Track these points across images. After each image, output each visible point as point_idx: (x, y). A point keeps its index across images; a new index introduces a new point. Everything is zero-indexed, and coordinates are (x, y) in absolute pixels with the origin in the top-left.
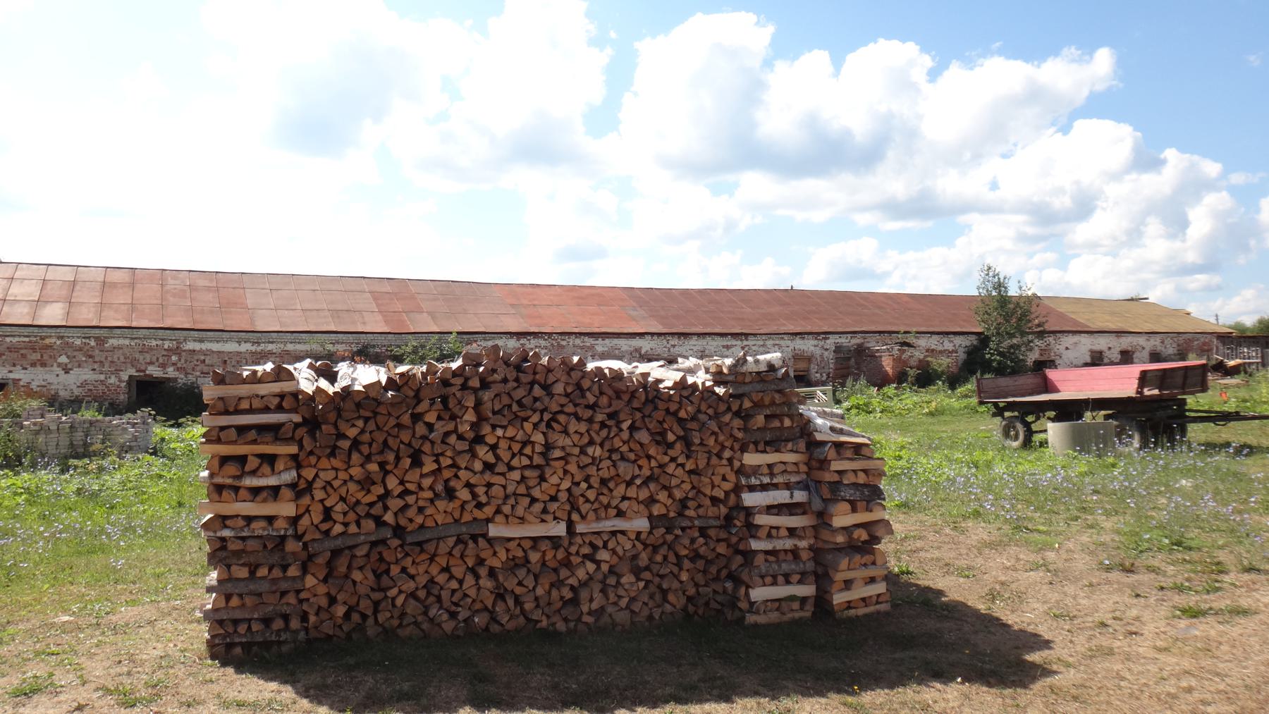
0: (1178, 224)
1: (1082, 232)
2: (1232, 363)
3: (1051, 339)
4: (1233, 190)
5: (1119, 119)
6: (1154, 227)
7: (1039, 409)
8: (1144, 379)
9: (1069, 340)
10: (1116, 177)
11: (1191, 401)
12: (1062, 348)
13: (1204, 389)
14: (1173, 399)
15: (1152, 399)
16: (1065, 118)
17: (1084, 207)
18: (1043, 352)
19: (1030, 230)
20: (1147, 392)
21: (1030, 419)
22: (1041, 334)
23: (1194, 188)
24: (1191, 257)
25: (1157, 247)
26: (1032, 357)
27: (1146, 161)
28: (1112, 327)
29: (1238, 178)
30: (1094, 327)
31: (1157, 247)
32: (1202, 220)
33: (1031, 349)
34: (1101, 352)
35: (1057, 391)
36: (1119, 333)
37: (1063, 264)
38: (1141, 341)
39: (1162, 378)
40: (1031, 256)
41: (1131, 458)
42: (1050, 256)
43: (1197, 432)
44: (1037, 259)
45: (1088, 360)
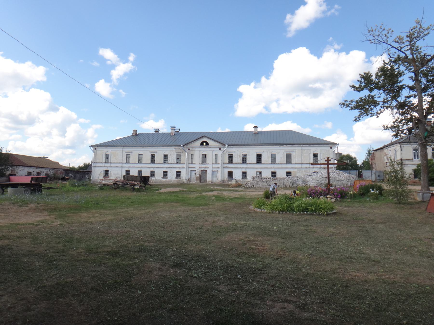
0: (63, 133)
1: (30, 130)
2: (67, 178)
3: (15, 167)
4: (81, 124)
5: (46, 90)
6: (55, 132)
7: (7, 186)
8: (32, 179)
9: (21, 168)
10: (43, 112)
11: (43, 185)
12: (18, 171)
13: (46, 182)
14: (39, 184)
15: (34, 184)
16: (27, 85)
17: (31, 121)
18: (12, 171)
19: (10, 125)
20: (33, 182)
21: (4, 188)
22: (12, 166)
23: (68, 122)
24: (67, 143)
25: (56, 139)
26: (8, 173)
27: (53, 108)
28: (35, 165)
29: (82, 120)
30: (30, 165)
31: (56, 139)
32: (72, 131)
33: (8, 170)
34: (31, 173)
35: (12, 182)
36: (46, 168)
37: (24, 139)
38: (44, 170)
39: (37, 179)
40: (11, 135)
41: (28, 196)
42: (19, 136)
43: (44, 191)
44: (13, 136)
45: (27, 174)
